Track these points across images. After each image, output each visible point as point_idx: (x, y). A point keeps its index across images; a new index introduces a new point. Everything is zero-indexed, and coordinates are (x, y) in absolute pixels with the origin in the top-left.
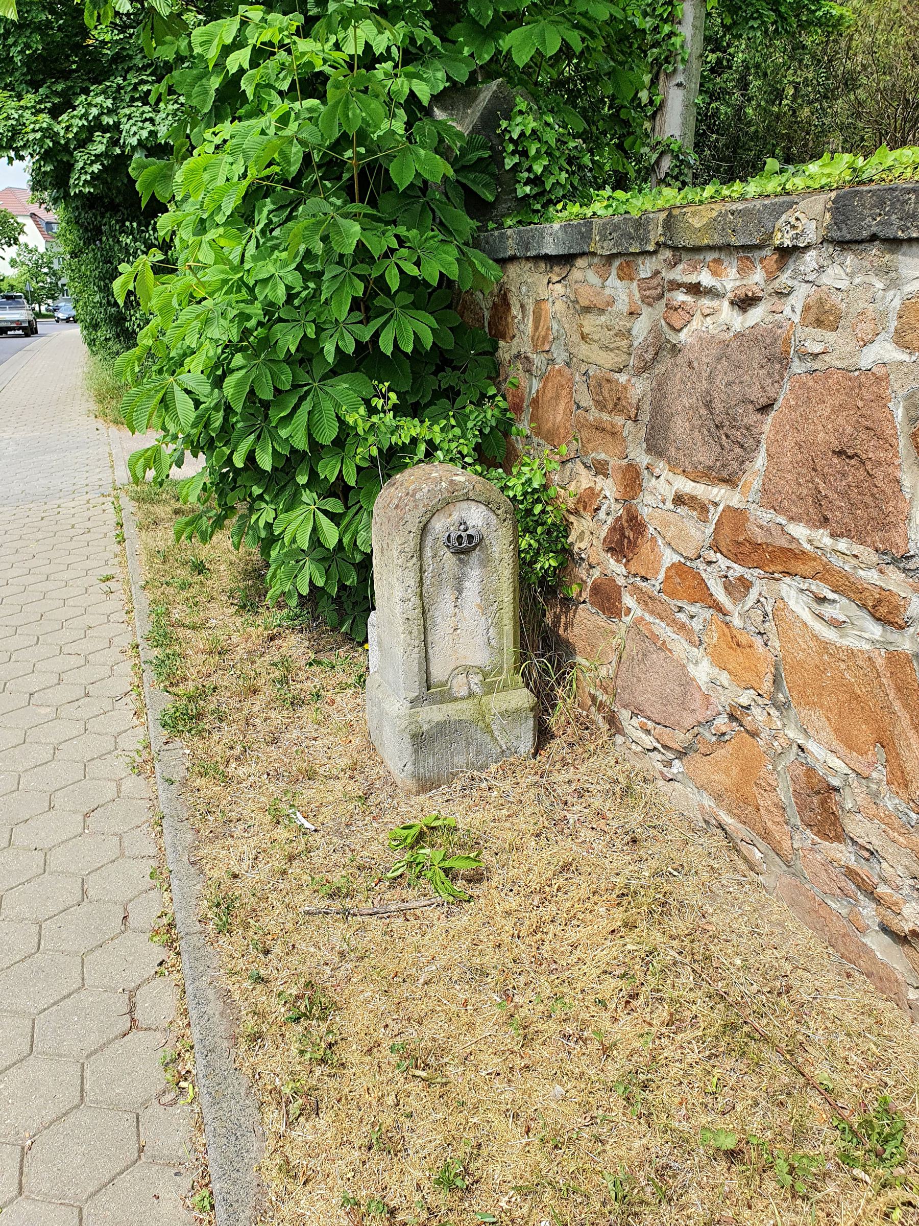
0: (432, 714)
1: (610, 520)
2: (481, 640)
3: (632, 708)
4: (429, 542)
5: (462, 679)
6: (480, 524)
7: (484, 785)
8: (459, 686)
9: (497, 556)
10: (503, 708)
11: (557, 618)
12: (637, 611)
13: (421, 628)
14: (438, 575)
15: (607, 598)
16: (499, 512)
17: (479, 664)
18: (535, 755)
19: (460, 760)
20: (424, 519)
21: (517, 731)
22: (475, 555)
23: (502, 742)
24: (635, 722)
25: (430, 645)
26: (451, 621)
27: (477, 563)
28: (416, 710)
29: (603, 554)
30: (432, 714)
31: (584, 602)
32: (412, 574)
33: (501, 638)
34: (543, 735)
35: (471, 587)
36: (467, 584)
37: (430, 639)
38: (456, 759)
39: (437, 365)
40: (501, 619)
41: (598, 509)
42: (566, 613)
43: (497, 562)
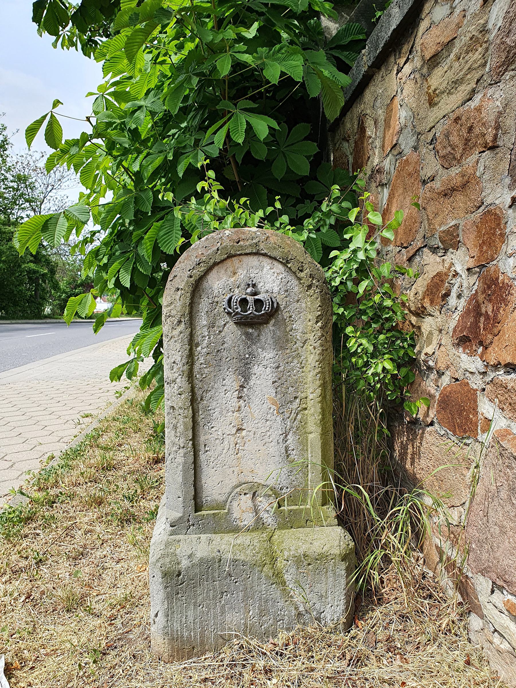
0: (199, 546)
1: (462, 304)
2: (275, 449)
3: (494, 576)
4: (204, 305)
5: (246, 501)
6: (276, 289)
7: (261, 663)
8: (242, 510)
10: (301, 551)
11: (404, 448)
12: (500, 423)
13: (189, 421)
15: (460, 414)
16: (302, 275)
17: (271, 482)
18: (349, 624)
19: (234, 619)
20: (197, 273)
21: (320, 588)
22: (269, 331)
23: (298, 599)
24: (498, 598)
25: (202, 447)
26: (233, 417)
27: (270, 341)
28: (177, 537)
29: (454, 351)
30: (199, 546)
31: (432, 424)
32: (178, 346)
33: (304, 450)
34: (361, 600)
35: (263, 376)
36: (256, 369)
37: (202, 439)
38: (228, 617)
39: (297, 199)
40: (304, 423)
41: (447, 295)
42: (413, 441)
43: (299, 344)
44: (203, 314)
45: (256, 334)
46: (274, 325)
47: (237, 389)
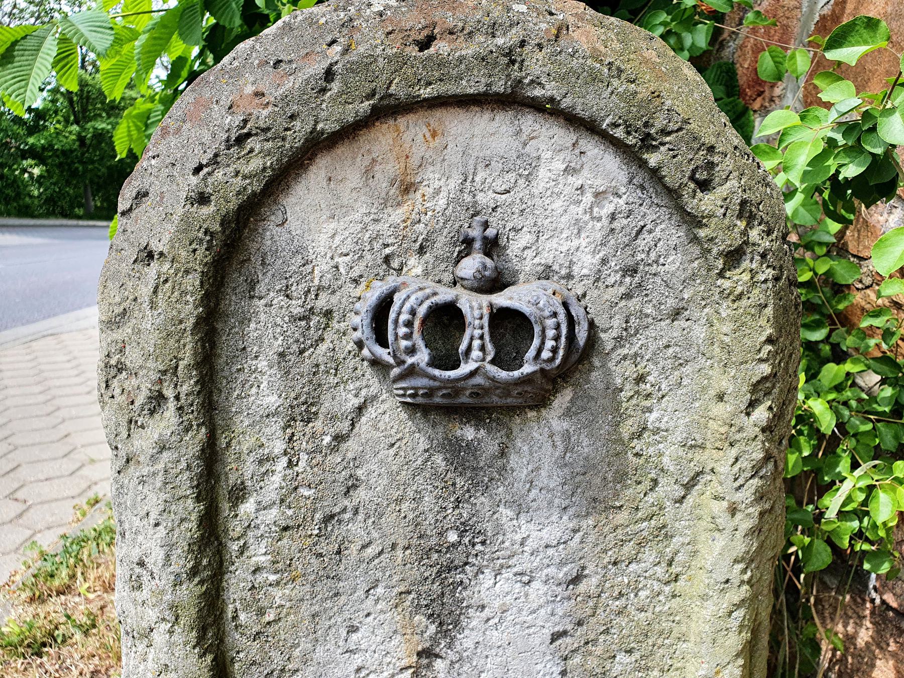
4: (265, 324)
6: (586, 263)
9: (669, 454)
14: (320, 526)
22: (541, 444)
27: (550, 476)
32: (154, 502)
36: (489, 589)
43: (668, 489)
44: (262, 364)
45: (491, 447)
46: (568, 413)
47: (405, 662)
